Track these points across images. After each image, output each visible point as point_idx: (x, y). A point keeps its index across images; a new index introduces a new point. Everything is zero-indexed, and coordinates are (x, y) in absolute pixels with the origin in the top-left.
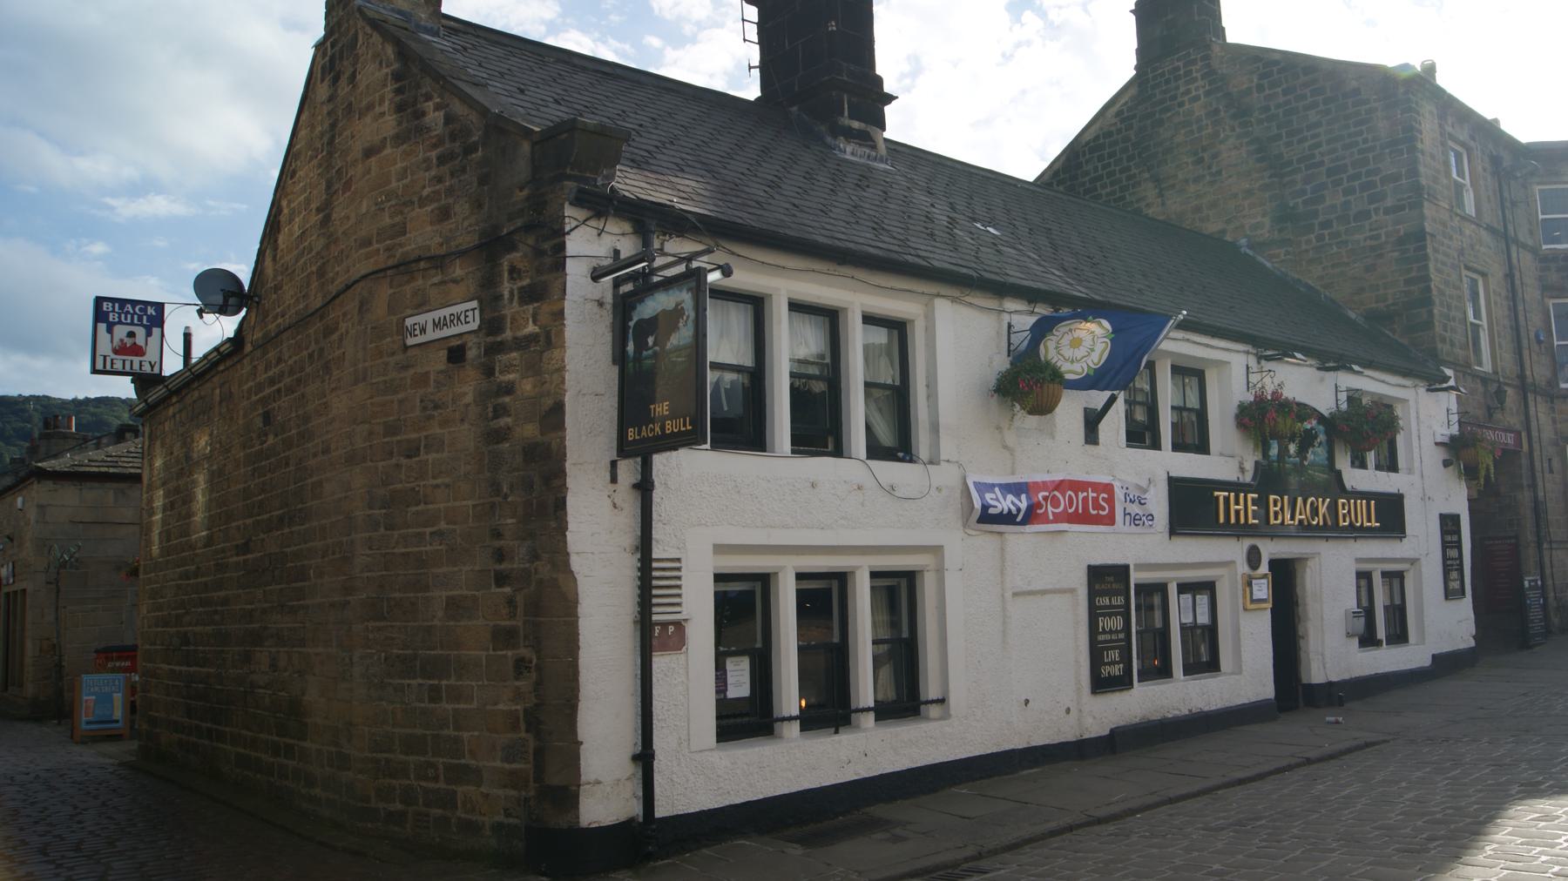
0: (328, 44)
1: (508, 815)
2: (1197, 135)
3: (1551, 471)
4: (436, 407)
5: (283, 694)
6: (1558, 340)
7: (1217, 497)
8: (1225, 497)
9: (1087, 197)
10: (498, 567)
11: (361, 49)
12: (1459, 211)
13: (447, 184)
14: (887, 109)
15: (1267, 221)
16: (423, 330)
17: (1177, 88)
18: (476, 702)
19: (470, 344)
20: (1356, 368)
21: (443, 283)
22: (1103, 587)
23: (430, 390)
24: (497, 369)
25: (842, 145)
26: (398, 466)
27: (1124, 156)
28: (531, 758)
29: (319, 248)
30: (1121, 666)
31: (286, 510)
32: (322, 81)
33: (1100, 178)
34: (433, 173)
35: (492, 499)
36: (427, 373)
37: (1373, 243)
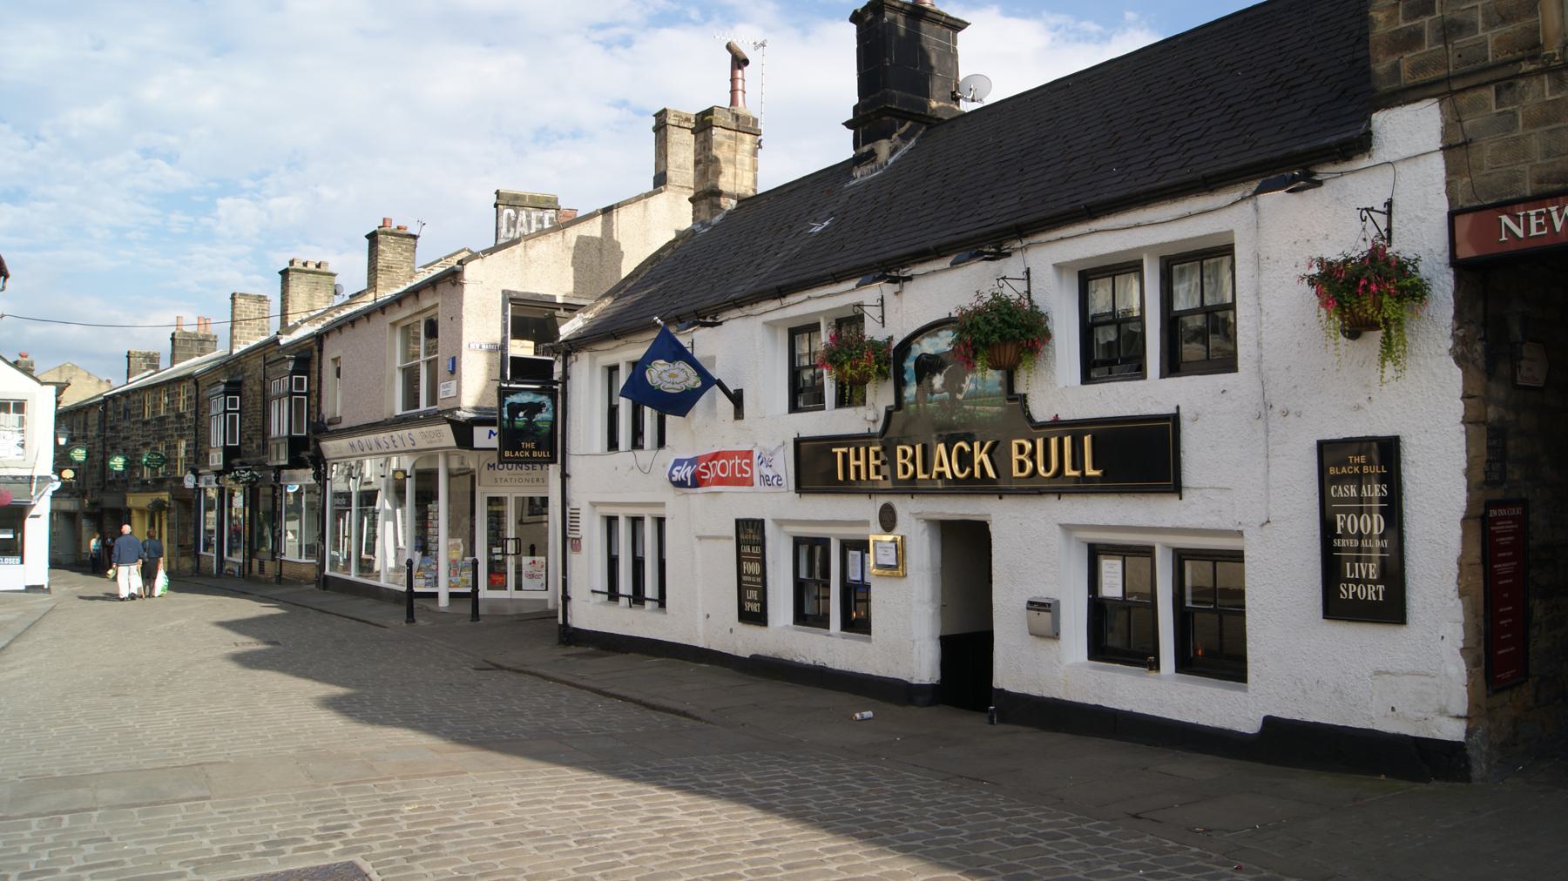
7: (836, 453)
22: (1344, 470)
30: (1381, 588)
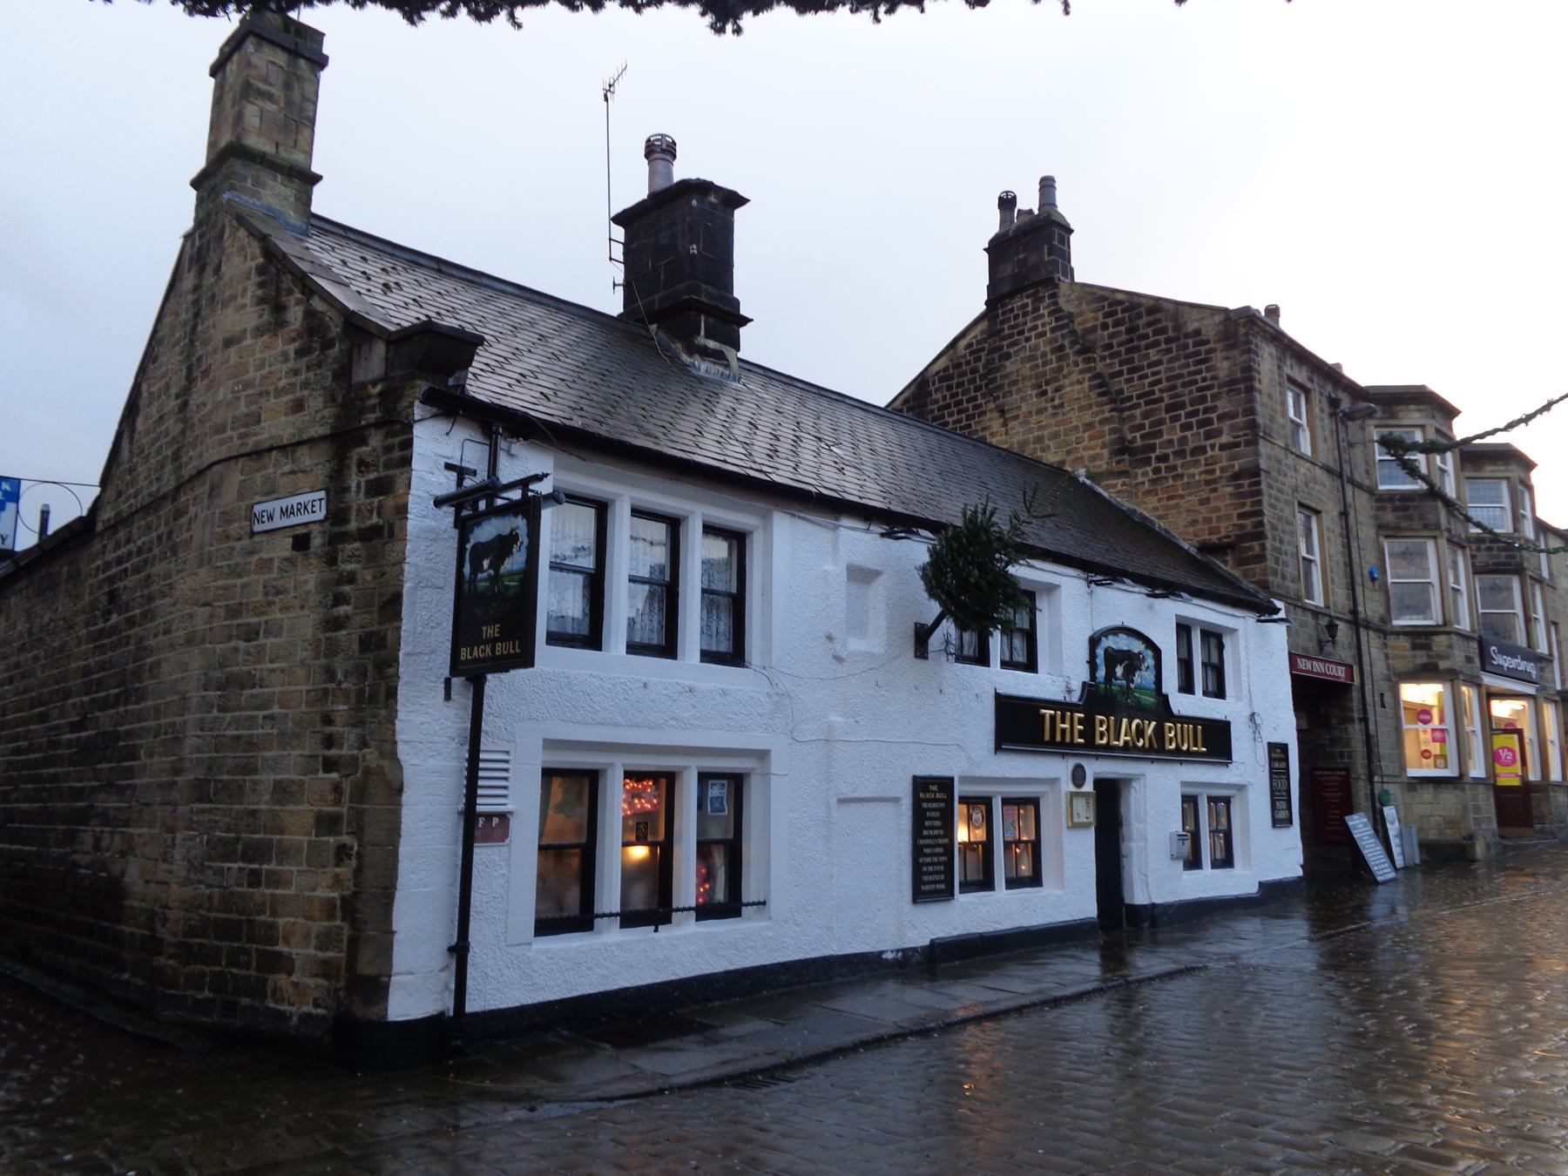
0: (197, 235)
1: (316, 1005)
3: (1383, 706)
4: (278, 593)
5: (103, 874)
8: (1051, 715)
9: (934, 424)
11: (227, 242)
12: (1293, 450)
14: (742, 330)
15: (1105, 452)
16: (271, 518)
17: (1025, 323)
21: (293, 472)
23: (275, 574)
26: (236, 649)
27: (972, 387)
28: (344, 946)
29: (176, 433)
31: (122, 688)
32: (189, 270)
33: (948, 406)
34: (290, 365)
35: (324, 685)
36: (271, 560)
37: (1209, 477)
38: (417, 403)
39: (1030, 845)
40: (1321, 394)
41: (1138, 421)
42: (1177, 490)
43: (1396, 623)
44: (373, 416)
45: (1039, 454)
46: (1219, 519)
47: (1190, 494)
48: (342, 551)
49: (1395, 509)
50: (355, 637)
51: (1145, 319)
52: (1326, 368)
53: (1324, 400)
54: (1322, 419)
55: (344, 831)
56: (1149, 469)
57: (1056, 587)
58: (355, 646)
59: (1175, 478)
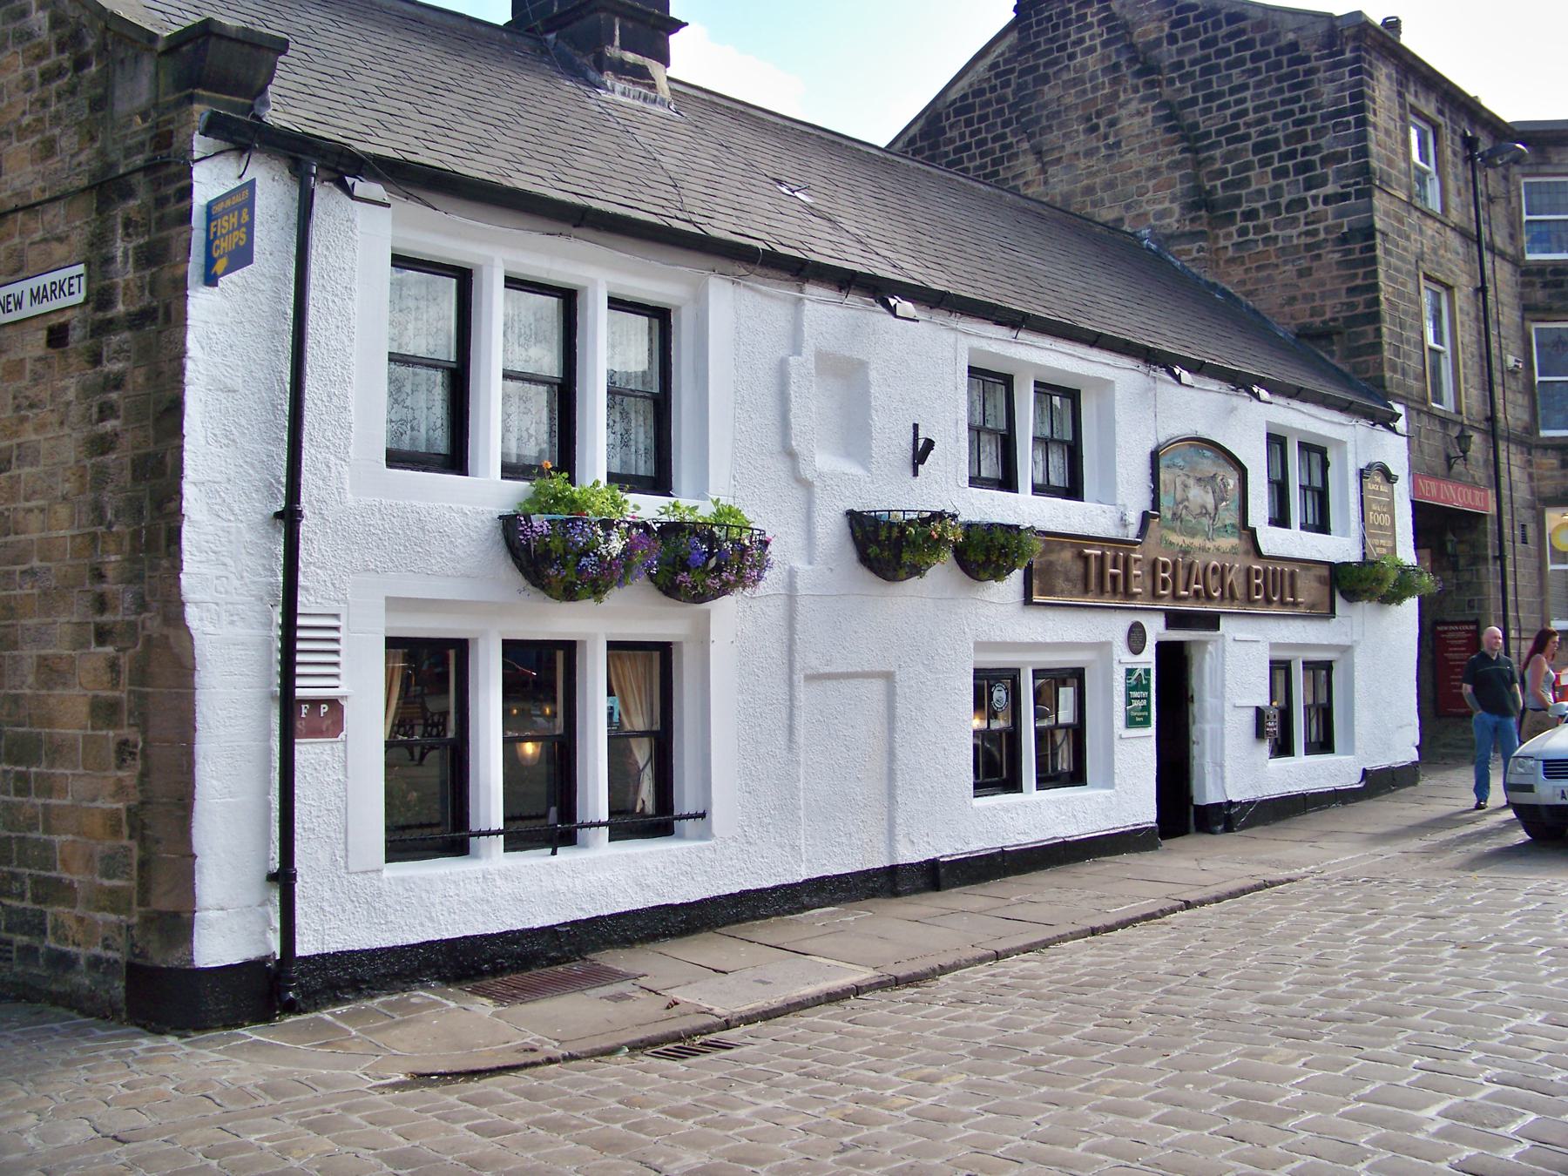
1: (107, 947)
2: (1090, 96)
3: (1524, 541)
4: (31, 406)
6: (1540, 375)
10: (98, 619)
12: (1418, 204)
13: (53, 109)
14: (672, 38)
15: (1176, 207)
16: (19, 304)
17: (1068, 35)
18: (70, 798)
19: (74, 322)
20: (1264, 394)
24: (105, 354)
25: (609, 84)
28: (135, 873)
33: (967, 147)
35: (93, 529)
36: (22, 360)
37: (1309, 240)
38: (197, 136)
39: (1071, 731)
40: (1454, 131)
41: (1217, 166)
42: (1269, 258)
43: (1544, 433)
44: (141, 157)
45: (1089, 209)
46: (1323, 296)
47: (1285, 263)
48: (108, 345)
49: (1545, 286)
50: (127, 461)
51: (1225, 30)
52: (1462, 99)
53: (1458, 140)
54: (1455, 165)
55: (126, 722)
56: (1233, 229)
57: (1110, 383)
58: (128, 474)
59: (1267, 241)
